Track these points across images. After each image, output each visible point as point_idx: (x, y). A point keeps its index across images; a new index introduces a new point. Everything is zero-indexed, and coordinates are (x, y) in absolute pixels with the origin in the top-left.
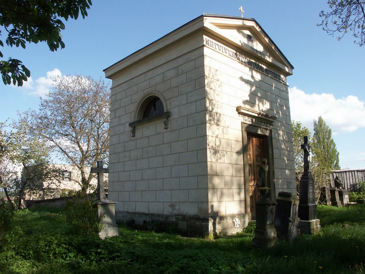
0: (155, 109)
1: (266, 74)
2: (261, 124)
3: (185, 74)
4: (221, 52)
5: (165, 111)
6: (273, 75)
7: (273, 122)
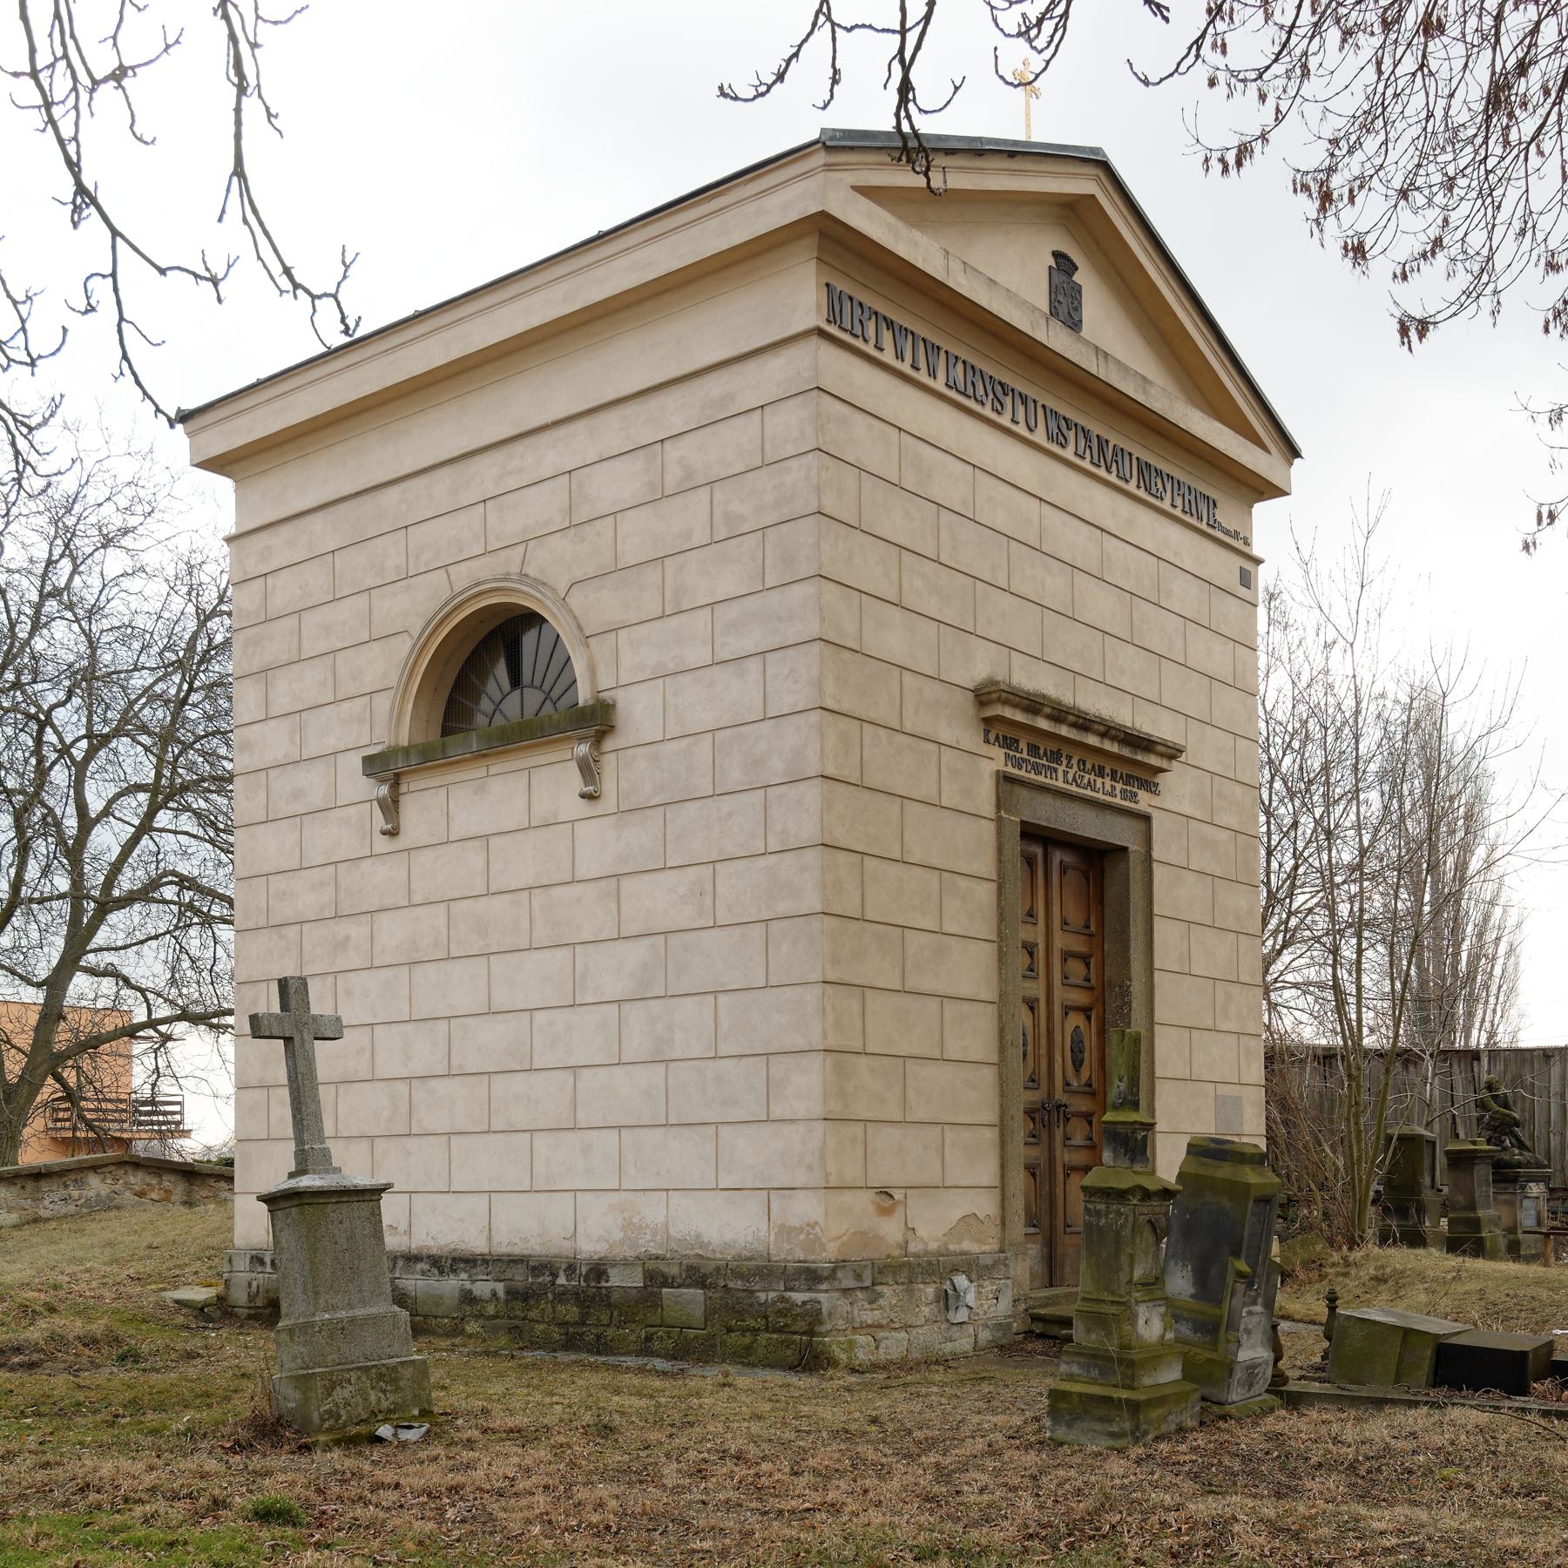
0: (516, 680)
1: (1142, 493)
2: (1099, 781)
3: (704, 494)
4: (905, 367)
5: (584, 695)
6: (1179, 501)
7: (1163, 770)
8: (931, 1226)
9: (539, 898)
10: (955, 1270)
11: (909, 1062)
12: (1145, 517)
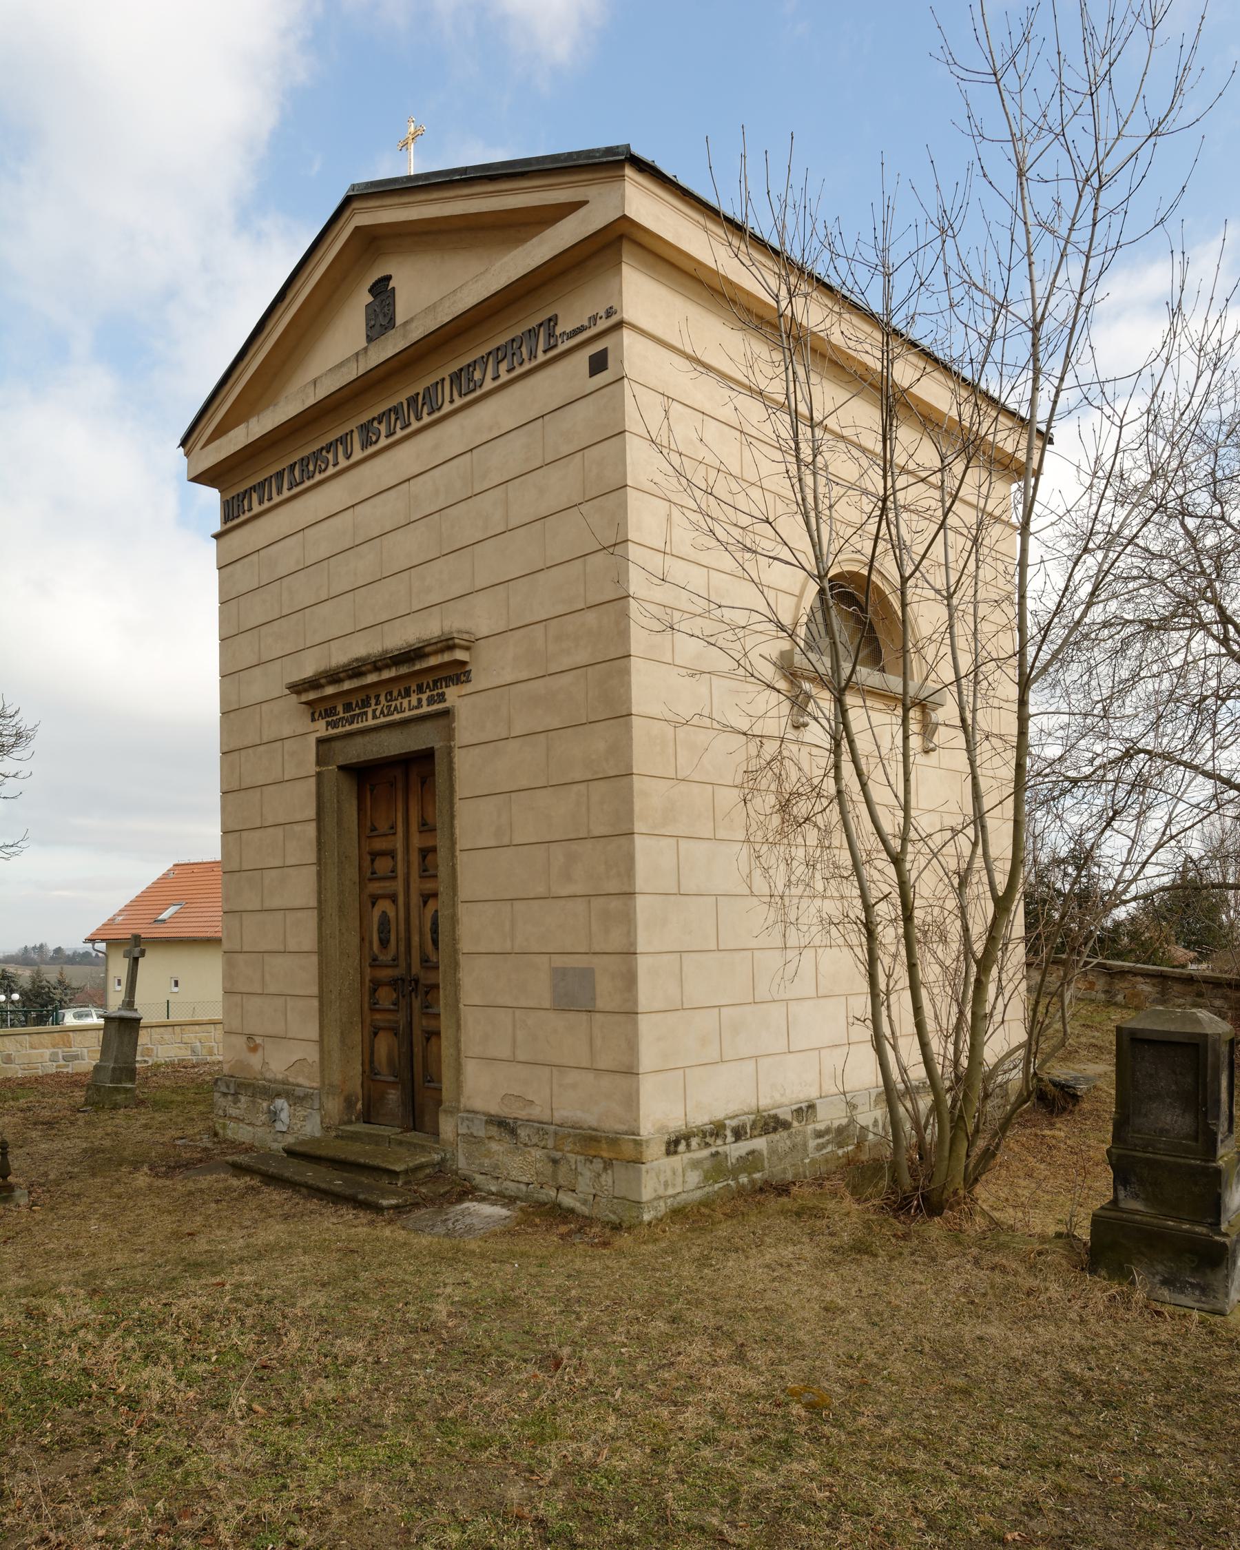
8: (277, 1063)
9: (506, 841)
10: (278, 1095)
11: (266, 956)
12: (451, 428)
